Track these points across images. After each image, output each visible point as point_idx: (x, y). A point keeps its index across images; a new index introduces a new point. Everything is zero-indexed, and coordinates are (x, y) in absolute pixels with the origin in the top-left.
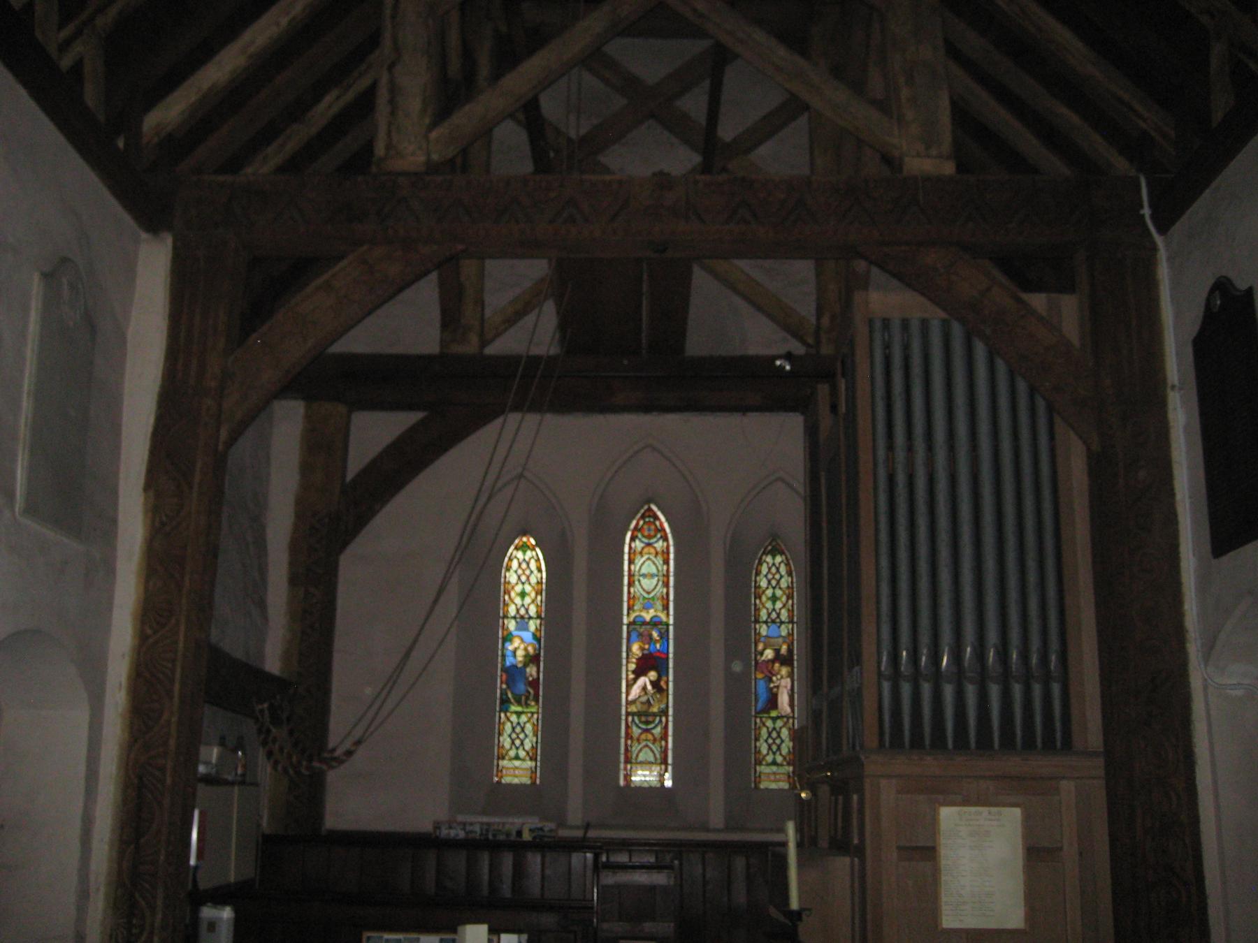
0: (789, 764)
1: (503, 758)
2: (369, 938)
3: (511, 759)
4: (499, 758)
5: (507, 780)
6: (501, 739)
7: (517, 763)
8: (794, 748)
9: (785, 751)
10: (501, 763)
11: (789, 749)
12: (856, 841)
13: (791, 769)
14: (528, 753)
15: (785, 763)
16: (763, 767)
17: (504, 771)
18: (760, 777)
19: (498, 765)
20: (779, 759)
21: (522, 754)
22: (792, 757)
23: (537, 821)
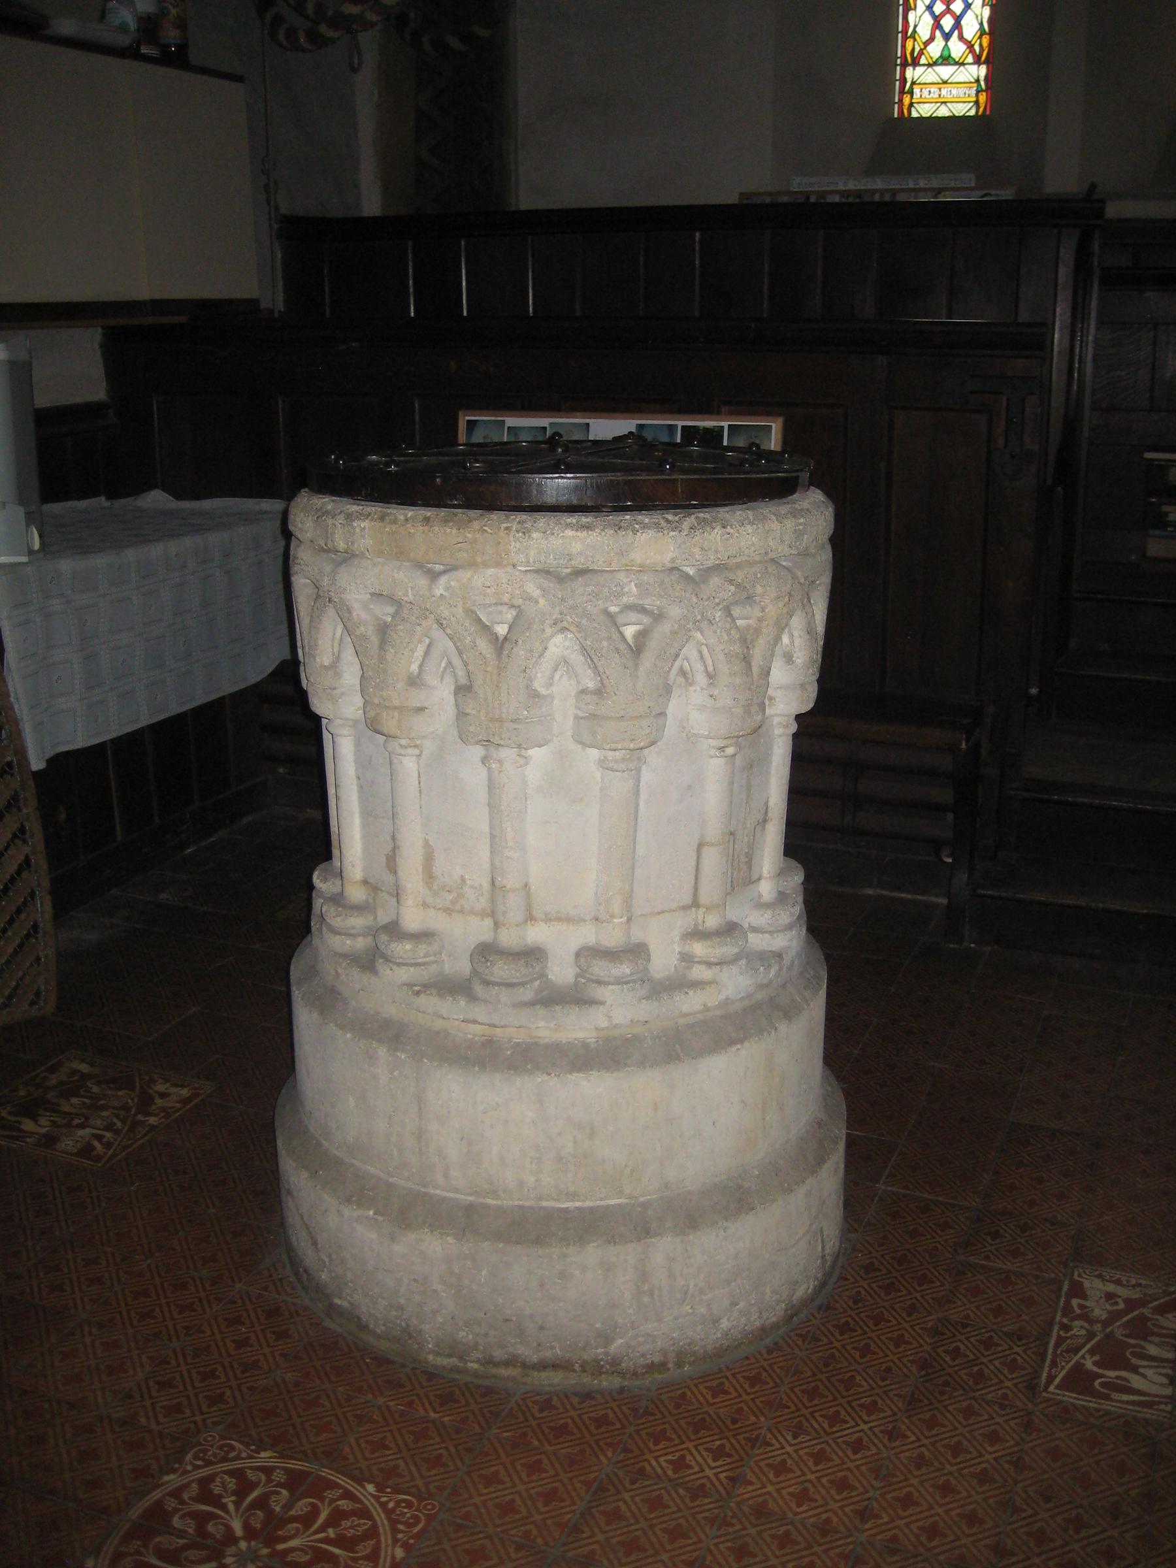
0: (977, 61)
1: (915, 63)
2: (471, 425)
3: (932, 65)
4: (904, 65)
5: (923, 110)
6: (911, 16)
7: (945, 71)
8: (991, 20)
9: (970, 28)
10: (910, 73)
11: (981, 24)
12: (183, 319)
13: (983, 71)
14: (970, 46)
15: (970, 59)
16: (920, 70)
17: (917, 90)
18: (911, 93)
19: (903, 80)
20: (957, 49)
21: (957, 49)
22: (986, 41)
23: (969, 179)
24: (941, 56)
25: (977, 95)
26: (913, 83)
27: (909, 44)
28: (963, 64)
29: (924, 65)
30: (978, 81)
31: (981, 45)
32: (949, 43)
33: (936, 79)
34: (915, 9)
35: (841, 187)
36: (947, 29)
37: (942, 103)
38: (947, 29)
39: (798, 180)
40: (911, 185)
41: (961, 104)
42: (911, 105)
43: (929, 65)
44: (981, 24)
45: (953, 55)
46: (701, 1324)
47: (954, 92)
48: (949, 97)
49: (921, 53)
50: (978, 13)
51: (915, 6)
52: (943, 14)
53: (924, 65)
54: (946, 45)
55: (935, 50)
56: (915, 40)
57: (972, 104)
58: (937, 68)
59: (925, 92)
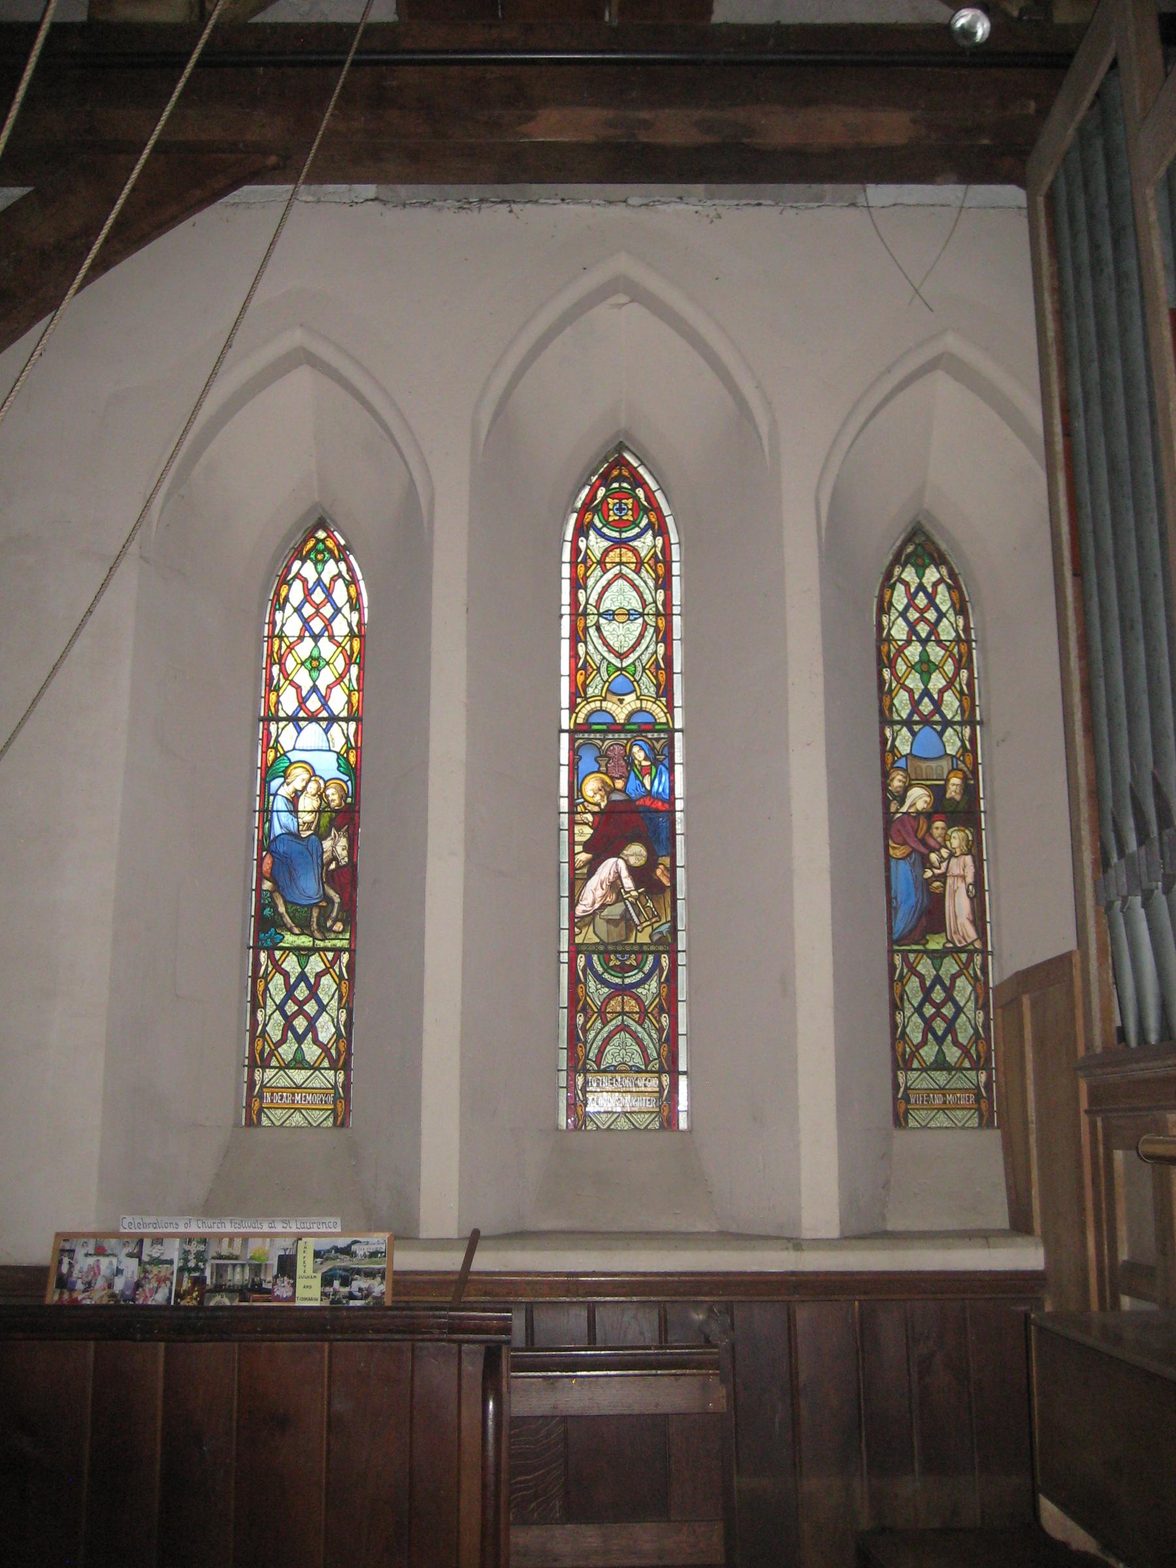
1: (266, 1065)
7: (299, 1076)
14: (325, 1048)
15: (326, 1064)
16: (270, 1073)
18: (261, 1096)
21: (312, 1052)
24: (294, 1059)
25: (334, 1103)
26: (263, 1086)
27: (259, 1044)
28: (319, 1069)
29: (274, 1067)
30: (335, 1087)
31: (337, 1049)
32: (319, 644)
33: (288, 1083)
34: (264, 1008)
35: (182, 1229)
36: (314, 697)
37: (296, 1109)
38: (314, 697)
39: (129, 1219)
40: (266, 1229)
41: (317, 1112)
42: (261, 1110)
43: (280, 1068)
44: (347, 738)
45: (308, 1058)
46: (147, 1278)
47: (309, 1098)
48: (304, 1104)
49: (271, 1054)
50: (334, 1014)
51: (265, 1003)
52: (312, 617)
53: (274, 1067)
54: (303, 969)
55: (287, 1051)
56: (265, 1040)
57: (330, 1112)
58: (290, 1072)
59: (277, 1098)
